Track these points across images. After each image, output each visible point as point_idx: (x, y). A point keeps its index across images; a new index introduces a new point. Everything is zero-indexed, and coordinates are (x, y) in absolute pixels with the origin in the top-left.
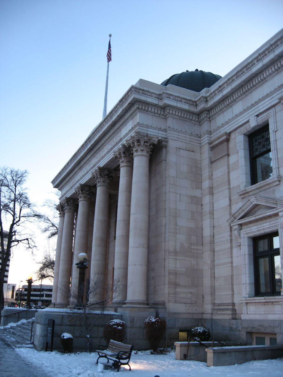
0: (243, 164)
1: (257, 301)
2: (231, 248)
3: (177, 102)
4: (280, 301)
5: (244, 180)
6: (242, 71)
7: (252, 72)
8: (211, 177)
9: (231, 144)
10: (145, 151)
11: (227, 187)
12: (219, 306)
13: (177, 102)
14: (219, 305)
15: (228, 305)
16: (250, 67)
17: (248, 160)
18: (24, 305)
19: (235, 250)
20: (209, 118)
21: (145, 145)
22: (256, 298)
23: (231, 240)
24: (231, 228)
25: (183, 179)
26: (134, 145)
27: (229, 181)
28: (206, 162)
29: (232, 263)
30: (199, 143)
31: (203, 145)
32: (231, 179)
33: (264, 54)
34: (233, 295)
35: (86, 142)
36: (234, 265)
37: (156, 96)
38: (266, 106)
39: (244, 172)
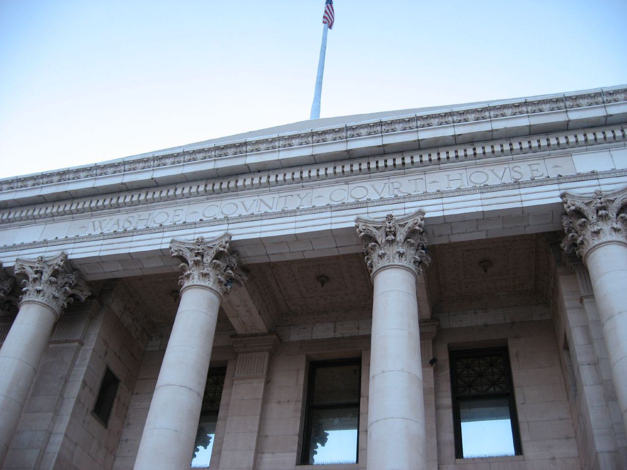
3: (605, 107)
6: (25, 183)
7: (183, 171)
10: (212, 280)
13: (605, 107)
16: (246, 152)
21: (66, 290)
26: (41, 278)
33: (287, 142)
35: (205, 142)
38: (314, 209)
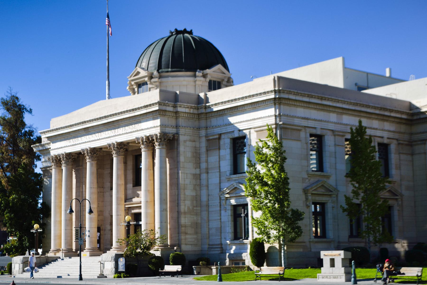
0: (229, 158)
1: (235, 243)
2: (220, 210)
4: (333, 195)
5: (229, 169)
8: (207, 162)
9: (222, 142)
11: (218, 170)
12: (212, 246)
14: (212, 245)
15: (218, 245)
17: (232, 155)
18: (131, 249)
19: (223, 212)
20: (206, 118)
22: (235, 241)
23: (220, 205)
24: (220, 198)
25: (188, 162)
27: (220, 167)
28: (203, 150)
29: (221, 219)
30: (198, 135)
31: (202, 136)
32: (221, 165)
34: (221, 239)
36: (222, 220)
37: (172, 105)
39: (229, 164)
